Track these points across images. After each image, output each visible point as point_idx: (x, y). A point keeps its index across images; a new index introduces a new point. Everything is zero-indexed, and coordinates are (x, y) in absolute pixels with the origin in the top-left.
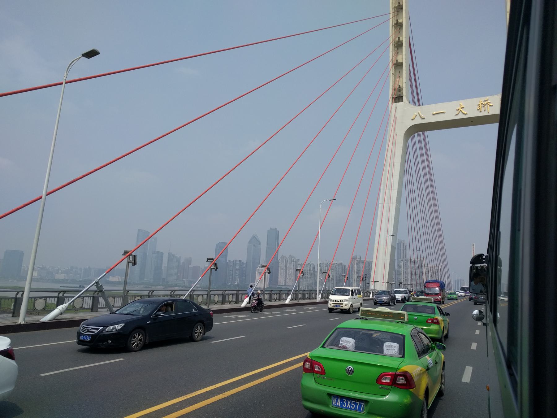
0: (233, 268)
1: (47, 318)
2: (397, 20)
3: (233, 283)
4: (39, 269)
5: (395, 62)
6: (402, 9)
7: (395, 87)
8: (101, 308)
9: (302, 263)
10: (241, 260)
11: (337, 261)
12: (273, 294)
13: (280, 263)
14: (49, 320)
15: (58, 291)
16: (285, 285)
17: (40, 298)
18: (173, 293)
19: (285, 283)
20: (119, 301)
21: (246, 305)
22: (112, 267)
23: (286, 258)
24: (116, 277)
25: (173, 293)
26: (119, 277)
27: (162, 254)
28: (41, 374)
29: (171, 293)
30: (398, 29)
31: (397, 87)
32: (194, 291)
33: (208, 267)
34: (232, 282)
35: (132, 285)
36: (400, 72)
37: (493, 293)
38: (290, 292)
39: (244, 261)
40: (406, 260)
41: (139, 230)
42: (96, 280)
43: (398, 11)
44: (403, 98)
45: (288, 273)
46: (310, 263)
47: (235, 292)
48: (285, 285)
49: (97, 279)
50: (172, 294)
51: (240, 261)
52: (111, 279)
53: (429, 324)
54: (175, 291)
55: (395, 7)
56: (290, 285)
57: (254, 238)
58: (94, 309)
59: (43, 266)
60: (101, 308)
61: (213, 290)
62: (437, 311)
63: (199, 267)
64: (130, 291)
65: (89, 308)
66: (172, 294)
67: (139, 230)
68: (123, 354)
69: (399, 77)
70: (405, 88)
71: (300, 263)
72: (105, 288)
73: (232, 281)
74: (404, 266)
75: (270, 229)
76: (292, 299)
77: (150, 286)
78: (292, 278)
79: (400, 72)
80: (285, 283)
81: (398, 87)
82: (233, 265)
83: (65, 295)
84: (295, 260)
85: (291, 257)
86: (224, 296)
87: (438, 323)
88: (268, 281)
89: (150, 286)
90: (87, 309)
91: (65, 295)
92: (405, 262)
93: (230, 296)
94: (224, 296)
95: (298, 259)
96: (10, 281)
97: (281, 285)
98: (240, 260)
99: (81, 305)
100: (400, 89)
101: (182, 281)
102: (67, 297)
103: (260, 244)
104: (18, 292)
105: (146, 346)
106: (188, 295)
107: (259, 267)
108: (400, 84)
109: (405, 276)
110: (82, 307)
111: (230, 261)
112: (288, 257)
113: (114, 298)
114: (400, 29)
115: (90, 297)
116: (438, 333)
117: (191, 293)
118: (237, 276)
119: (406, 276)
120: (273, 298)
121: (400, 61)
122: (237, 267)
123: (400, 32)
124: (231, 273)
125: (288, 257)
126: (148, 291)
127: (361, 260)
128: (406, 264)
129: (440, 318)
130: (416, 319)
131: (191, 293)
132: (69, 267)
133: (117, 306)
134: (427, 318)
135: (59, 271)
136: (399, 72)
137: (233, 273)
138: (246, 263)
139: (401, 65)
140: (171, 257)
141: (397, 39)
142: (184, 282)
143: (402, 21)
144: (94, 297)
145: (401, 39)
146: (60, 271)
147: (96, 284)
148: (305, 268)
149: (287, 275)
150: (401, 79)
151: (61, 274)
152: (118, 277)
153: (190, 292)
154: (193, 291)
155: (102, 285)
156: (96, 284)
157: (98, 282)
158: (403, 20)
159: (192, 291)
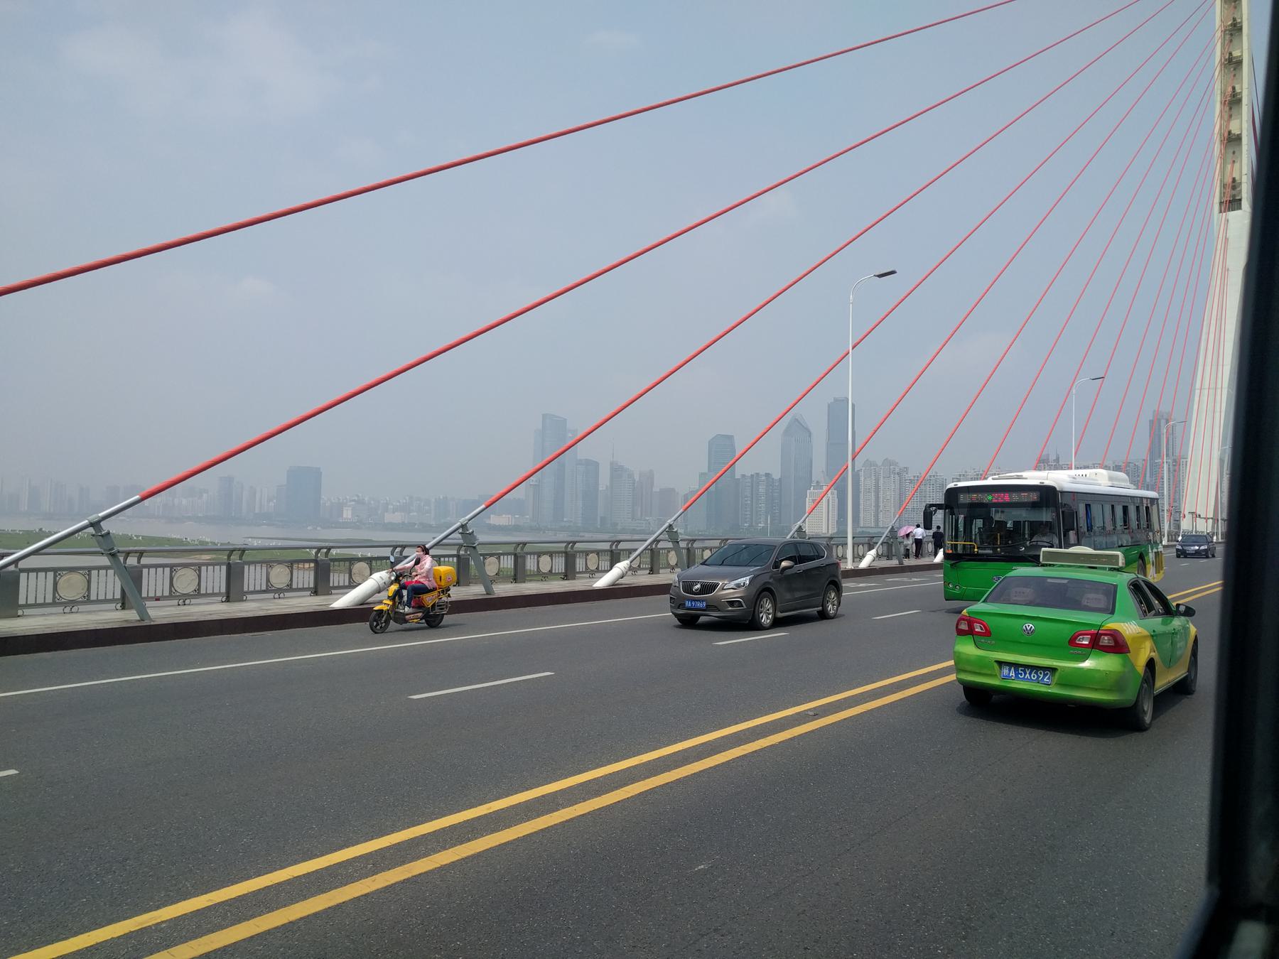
0: (752, 491)
1: (603, 582)
2: (1230, 54)
3: (754, 524)
4: (353, 503)
5: (1226, 134)
6: (1240, 29)
7: (1226, 181)
8: (580, 573)
9: (914, 476)
10: (769, 474)
11: (999, 468)
12: (834, 547)
13: (862, 479)
14: (351, 604)
15: (565, 542)
16: (877, 526)
17: (72, 570)
18: (522, 549)
19: (877, 521)
20: (258, 576)
21: (871, 563)
22: (496, 495)
23: (877, 466)
24: (504, 516)
25: (617, 546)
26: (510, 516)
27: (597, 464)
28: (551, 675)
29: (611, 546)
30: (1232, 69)
31: (1228, 180)
32: (659, 541)
33: (697, 491)
34: (752, 523)
35: (544, 532)
36: (1234, 153)
37: (954, 524)
38: (874, 540)
39: (776, 475)
40: (1174, 461)
41: (544, 416)
42: (463, 520)
43: (1231, 35)
44: (1240, 204)
45: (881, 500)
46: (964, 475)
47: (606, 546)
48: (877, 526)
49: (94, 516)
50: (614, 547)
51: (767, 475)
52: (495, 519)
53: (1079, 650)
54: (619, 542)
55: (1225, 31)
56: (867, 525)
57: (796, 423)
58: (655, 569)
59: (358, 496)
60: (580, 573)
61: (628, 537)
62: (1125, 599)
63: (673, 490)
64: (529, 543)
65: (113, 601)
66: (614, 547)
67: (544, 416)
68: (747, 632)
69: (1234, 162)
70: (1246, 184)
71: (910, 475)
72: (482, 538)
73: (752, 519)
74: (1171, 475)
75: (832, 401)
76: (878, 556)
77: (582, 534)
78: (893, 509)
79: (1234, 153)
80: (877, 521)
81: (1231, 180)
82: (752, 484)
83: (144, 561)
84: (897, 470)
85: (888, 463)
86: (519, 559)
87: (1118, 645)
88: (836, 518)
89: (582, 534)
90: (303, 589)
91: (144, 561)
92: (1174, 465)
93: (591, 555)
94: (519, 559)
95: (906, 468)
96: (309, 528)
97: (869, 527)
98: (766, 474)
99: (549, 569)
100: (1235, 184)
101: (644, 522)
102: (149, 567)
103: (810, 436)
104: (395, 547)
105: (777, 623)
106: (645, 549)
107: (812, 489)
108: (1234, 176)
109: (1174, 499)
110: (550, 571)
111: (743, 476)
112: (880, 464)
113: (551, 556)
114: (1235, 69)
115: (220, 564)
116: (1118, 683)
117: (654, 546)
118: (763, 509)
119: (1177, 497)
120: (834, 554)
121: (1235, 131)
122: (762, 489)
123: (1235, 76)
124: (749, 502)
125: (880, 464)
126: (565, 542)
127: (1060, 463)
128: (1175, 471)
129: (1129, 626)
130: (1030, 632)
131: (654, 546)
132: (407, 498)
133: (557, 572)
134: (1068, 631)
135: (389, 507)
136: (1232, 151)
137: (752, 502)
138: (780, 479)
139: (1238, 139)
140: (617, 470)
141: (1230, 89)
142: (649, 523)
143: (1240, 54)
144: (229, 566)
145: (1238, 90)
146: (391, 507)
147: (460, 531)
148: (922, 487)
149: (881, 504)
150: (1237, 165)
151: (394, 513)
152: (507, 516)
153: (651, 544)
154: (657, 541)
155: (473, 532)
156: (460, 531)
157: (466, 524)
158: (1242, 52)
159: (654, 541)
